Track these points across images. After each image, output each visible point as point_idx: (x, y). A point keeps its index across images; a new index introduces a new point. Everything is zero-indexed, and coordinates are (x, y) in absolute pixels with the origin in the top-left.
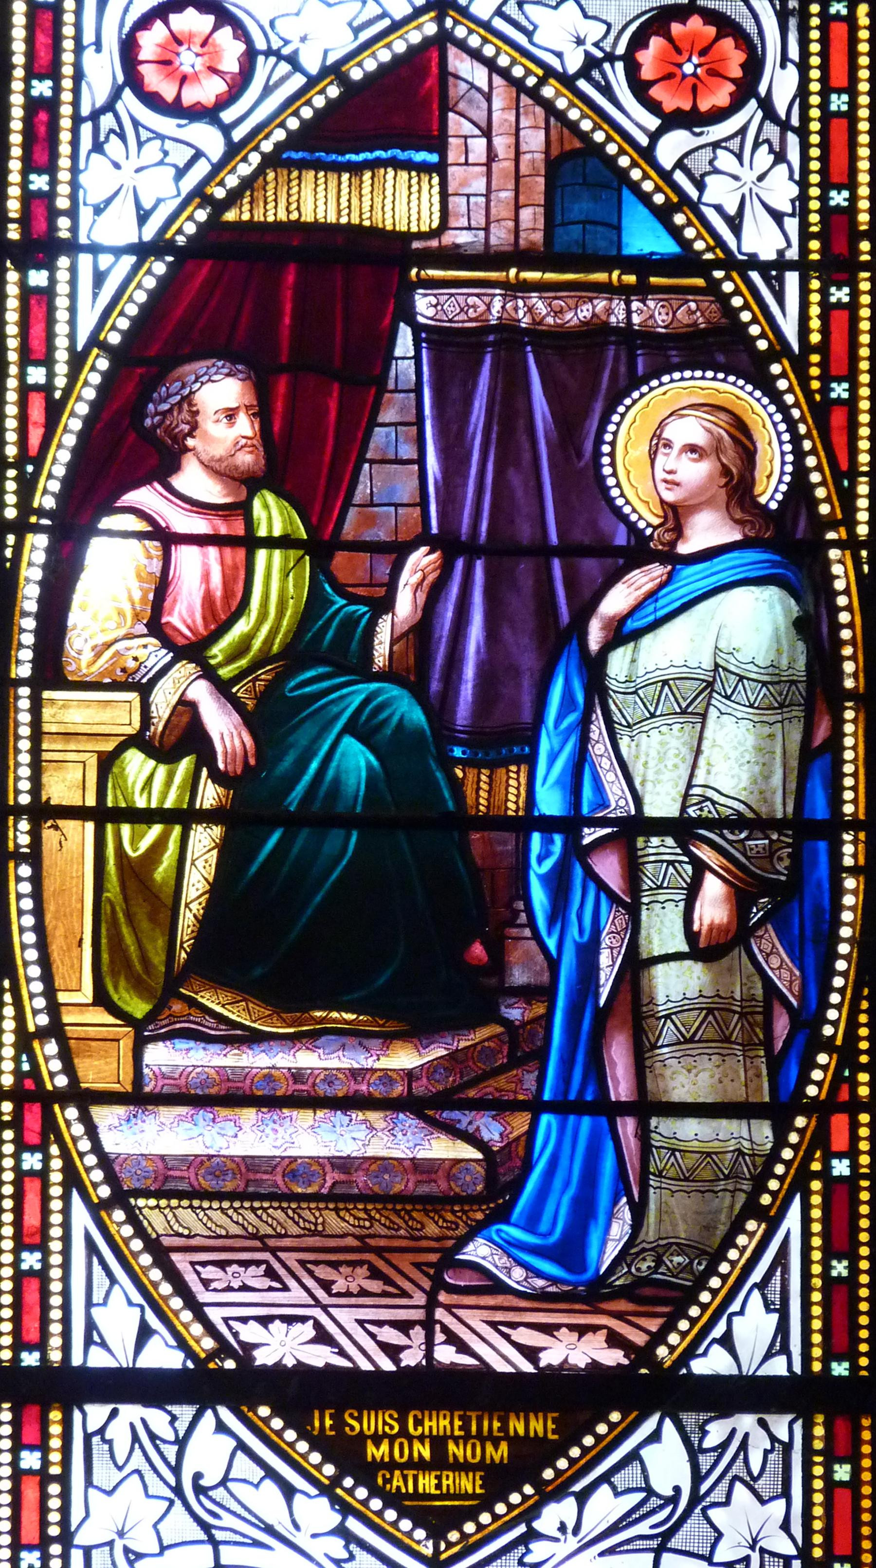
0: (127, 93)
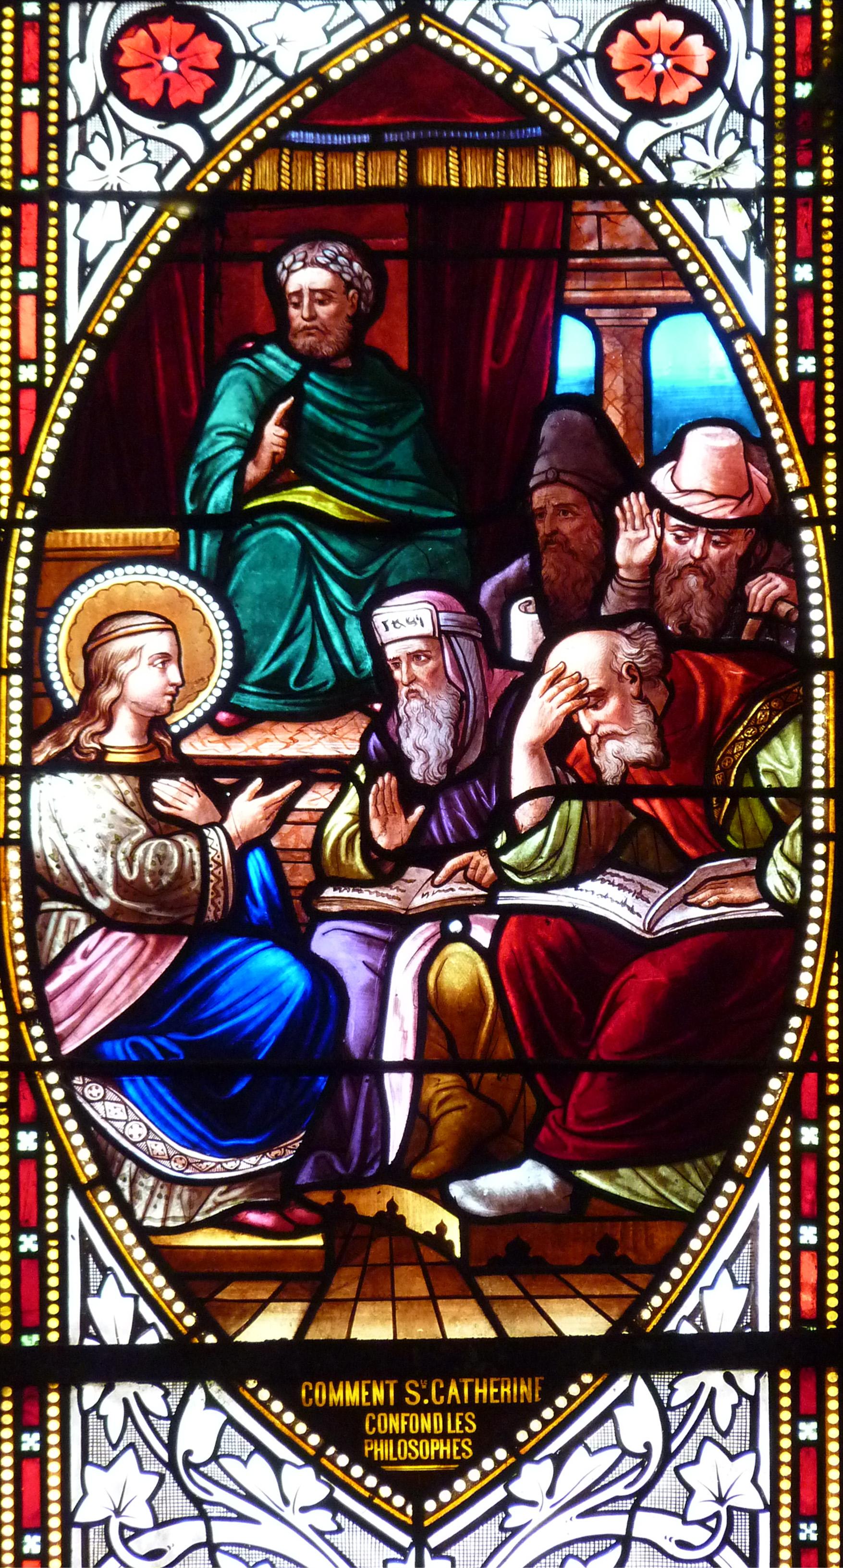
0: (112, 100)
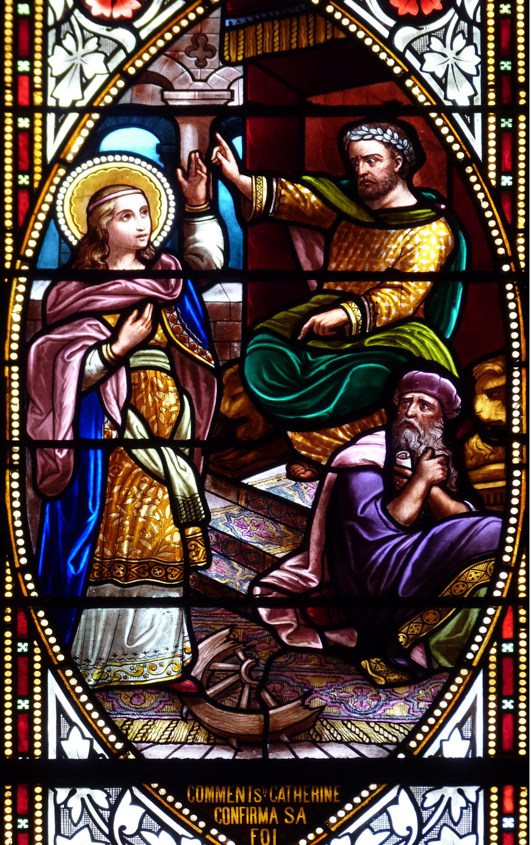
0: (77, 12)
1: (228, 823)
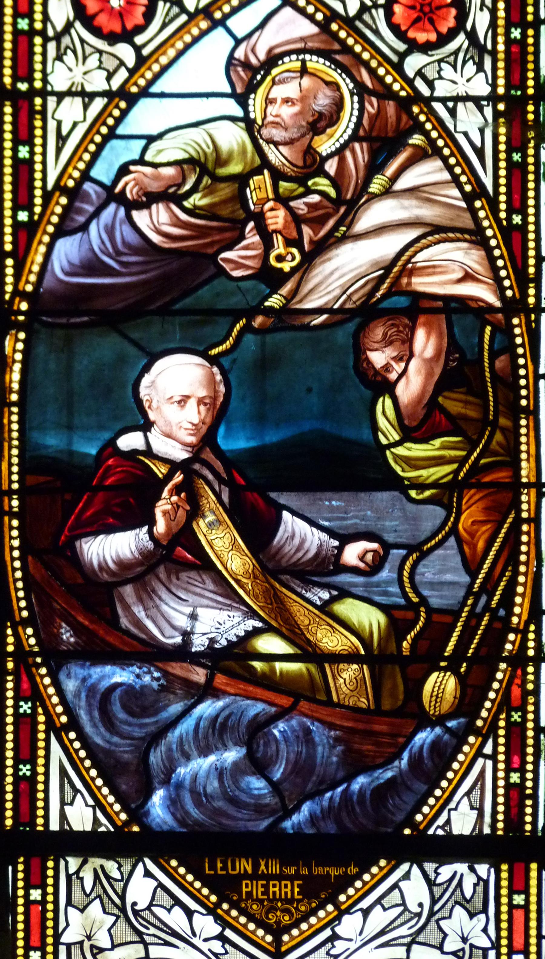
1: (237, 872)
